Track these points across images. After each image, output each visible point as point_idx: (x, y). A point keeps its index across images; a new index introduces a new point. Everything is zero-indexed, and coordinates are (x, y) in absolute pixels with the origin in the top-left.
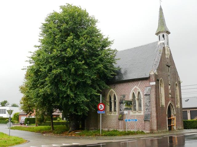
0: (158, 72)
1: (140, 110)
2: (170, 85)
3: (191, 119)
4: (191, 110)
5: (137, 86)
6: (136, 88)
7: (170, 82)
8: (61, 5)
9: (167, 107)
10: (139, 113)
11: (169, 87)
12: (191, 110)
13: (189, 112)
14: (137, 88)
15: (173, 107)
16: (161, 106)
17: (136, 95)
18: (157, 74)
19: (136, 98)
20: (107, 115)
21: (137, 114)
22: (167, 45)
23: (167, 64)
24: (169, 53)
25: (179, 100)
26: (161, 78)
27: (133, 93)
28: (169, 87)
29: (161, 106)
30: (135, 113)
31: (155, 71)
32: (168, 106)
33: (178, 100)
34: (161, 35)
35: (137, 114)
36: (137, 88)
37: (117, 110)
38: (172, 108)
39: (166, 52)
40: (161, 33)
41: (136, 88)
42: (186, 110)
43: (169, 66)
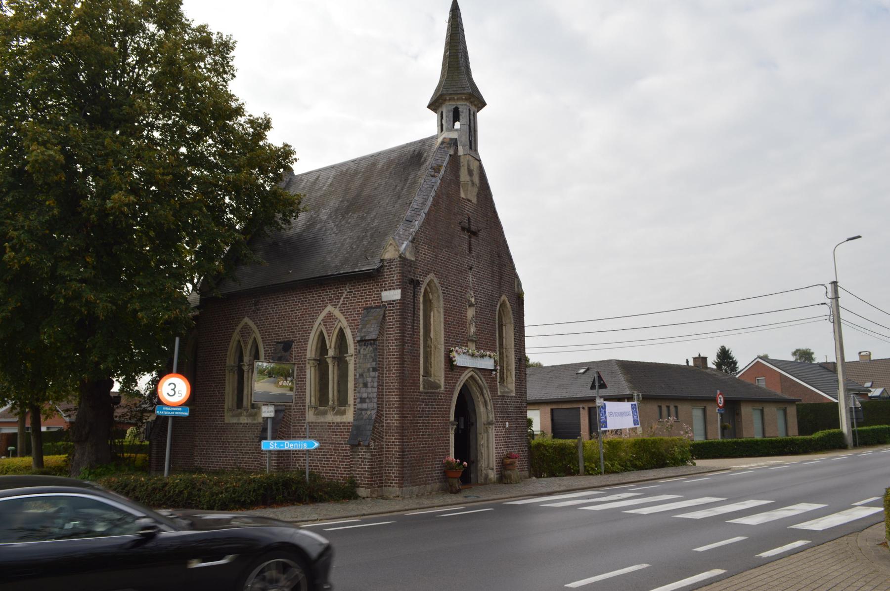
0: (416, 250)
1: (343, 400)
2: (471, 305)
3: (801, 431)
4: (554, 407)
5: (335, 306)
6: (330, 315)
7: (472, 292)
8: (794, 350)
9: (453, 389)
10: (336, 414)
11: (471, 313)
12: (554, 407)
13: (586, 408)
14: (337, 313)
15: (482, 394)
16: (421, 389)
17: (331, 343)
18: (409, 256)
19: (331, 353)
20: (226, 421)
21: (330, 418)
22: (468, 147)
23: (467, 225)
24: (476, 179)
25: (513, 367)
26: (431, 276)
27: (322, 332)
28: (471, 313)
29: (421, 389)
30: (324, 413)
31: (404, 246)
32: (458, 389)
33: (508, 365)
34: (447, 109)
35: (330, 418)
36: (337, 313)
37: (351, 400)
38: (481, 399)
39: (464, 176)
40: (447, 103)
41: (330, 315)
42: (575, 406)
43: (475, 234)
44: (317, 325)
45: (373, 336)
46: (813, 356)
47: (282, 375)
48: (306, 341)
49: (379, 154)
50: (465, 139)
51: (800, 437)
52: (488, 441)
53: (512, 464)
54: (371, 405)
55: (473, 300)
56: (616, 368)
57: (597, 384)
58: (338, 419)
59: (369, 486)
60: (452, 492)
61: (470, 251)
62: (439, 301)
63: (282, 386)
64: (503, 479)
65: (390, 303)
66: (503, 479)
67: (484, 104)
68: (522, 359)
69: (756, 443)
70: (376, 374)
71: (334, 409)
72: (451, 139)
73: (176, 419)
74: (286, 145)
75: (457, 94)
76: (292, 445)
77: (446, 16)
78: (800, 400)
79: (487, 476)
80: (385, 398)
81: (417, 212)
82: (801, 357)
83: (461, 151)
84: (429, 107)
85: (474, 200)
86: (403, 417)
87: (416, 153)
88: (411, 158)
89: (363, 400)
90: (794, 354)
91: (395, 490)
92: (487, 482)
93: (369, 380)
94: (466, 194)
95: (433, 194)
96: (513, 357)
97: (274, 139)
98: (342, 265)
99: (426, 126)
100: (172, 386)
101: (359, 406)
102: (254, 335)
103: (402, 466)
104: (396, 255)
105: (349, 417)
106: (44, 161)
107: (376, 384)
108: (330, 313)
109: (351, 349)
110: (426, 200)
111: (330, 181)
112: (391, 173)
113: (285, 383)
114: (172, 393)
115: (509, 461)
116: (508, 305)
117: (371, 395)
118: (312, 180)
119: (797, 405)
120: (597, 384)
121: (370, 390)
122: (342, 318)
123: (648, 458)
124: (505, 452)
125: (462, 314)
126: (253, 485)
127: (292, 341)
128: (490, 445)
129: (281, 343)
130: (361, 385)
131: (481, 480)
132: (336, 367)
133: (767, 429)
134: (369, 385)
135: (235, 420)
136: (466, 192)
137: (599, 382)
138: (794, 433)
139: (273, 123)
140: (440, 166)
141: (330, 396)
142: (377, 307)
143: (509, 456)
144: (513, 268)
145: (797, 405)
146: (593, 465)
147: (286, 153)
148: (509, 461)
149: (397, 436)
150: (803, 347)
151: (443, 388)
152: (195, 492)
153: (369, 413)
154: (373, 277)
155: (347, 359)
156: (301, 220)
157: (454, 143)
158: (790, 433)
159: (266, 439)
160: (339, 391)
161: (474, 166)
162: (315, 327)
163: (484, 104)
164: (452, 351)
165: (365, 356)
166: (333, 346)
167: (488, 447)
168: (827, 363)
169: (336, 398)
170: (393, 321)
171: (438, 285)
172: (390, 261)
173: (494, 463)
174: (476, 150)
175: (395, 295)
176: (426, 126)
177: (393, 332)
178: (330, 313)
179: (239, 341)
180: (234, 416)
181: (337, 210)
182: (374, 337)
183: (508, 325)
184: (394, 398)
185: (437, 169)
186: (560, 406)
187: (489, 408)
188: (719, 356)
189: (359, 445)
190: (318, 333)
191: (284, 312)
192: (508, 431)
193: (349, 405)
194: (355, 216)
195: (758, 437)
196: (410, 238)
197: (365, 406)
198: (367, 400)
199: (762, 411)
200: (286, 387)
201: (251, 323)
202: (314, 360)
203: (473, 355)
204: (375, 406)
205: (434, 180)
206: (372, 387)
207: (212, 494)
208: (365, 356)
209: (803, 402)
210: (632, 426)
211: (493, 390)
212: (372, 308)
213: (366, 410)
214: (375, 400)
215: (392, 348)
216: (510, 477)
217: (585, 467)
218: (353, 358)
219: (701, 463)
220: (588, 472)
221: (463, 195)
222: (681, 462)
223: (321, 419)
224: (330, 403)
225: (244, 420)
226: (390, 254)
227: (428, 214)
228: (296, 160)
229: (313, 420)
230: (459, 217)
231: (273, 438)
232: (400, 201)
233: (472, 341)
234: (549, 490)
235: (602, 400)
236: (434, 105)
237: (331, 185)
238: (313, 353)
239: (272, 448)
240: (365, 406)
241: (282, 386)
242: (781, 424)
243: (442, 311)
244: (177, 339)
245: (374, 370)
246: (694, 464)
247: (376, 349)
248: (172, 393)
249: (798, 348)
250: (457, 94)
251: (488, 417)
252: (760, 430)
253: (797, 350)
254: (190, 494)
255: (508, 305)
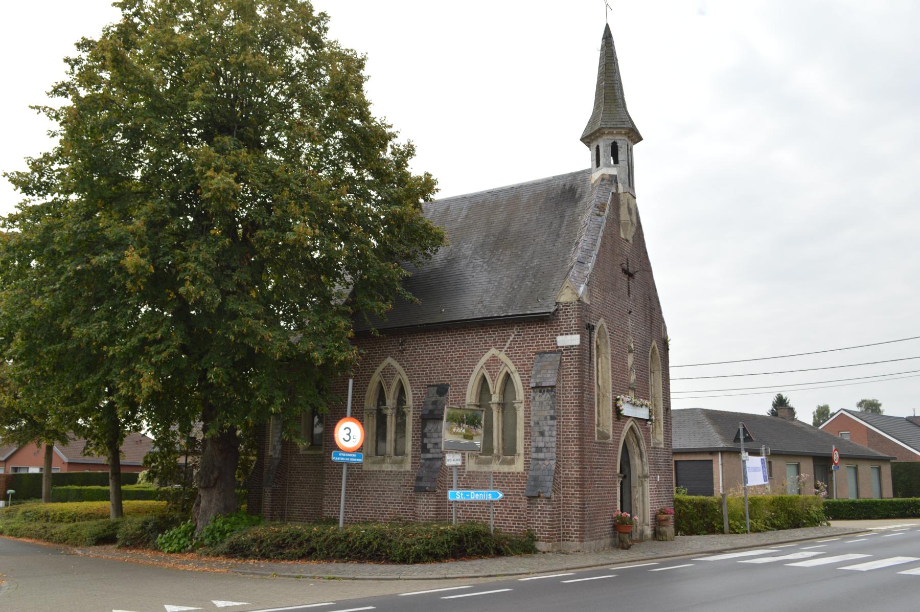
1: (510, 450)
2: (631, 351)
5: (500, 349)
6: (494, 359)
7: (631, 338)
11: (630, 359)
14: (502, 356)
15: (639, 445)
18: (586, 300)
19: (495, 398)
26: (602, 321)
28: (630, 359)
30: (488, 462)
34: (604, 144)
36: (502, 356)
38: (637, 450)
40: (605, 137)
41: (494, 359)
44: (478, 369)
45: (551, 383)
46: (881, 408)
47: (455, 421)
48: (465, 386)
49: (521, 187)
50: (623, 176)
51: (895, 499)
52: (643, 495)
53: (666, 520)
54: (548, 455)
55: (632, 346)
56: (703, 417)
57: (742, 437)
58: (505, 469)
59: (549, 540)
60: (623, 548)
61: (629, 294)
62: (607, 347)
63: (455, 433)
64: (657, 535)
65: (567, 348)
66: (657, 535)
67: (640, 139)
68: (667, 409)
69: (875, 504)
70: (555, 423)
71: (499, 457)
72: (611, 176)
73: (350, 465)
74: (428, 175)
75: (611, 128)
76: (477, 495)
77: (598, 42)
78: (895, 458)
79: (642, 533)
80: (563, 448)
81: (587, 252)
82: (867, 409)
83: (621, 190)
84: (583, 140)
85: (631, 241)
86: (583, 468)
87: (567, 187)
88: (564, 194)
89: (539, 450)
90: (860, 405)
91: (576, 544)
92: (642, 539)
93: (547, 428)
94: (625, 234)
95: (601, 234)
96: (662, 406)
97: (415, 168)
98: (508, 306)
99: (580, 159)
100: (348, 431)
101: (534, 455)
102: (398, 377)
103: (583, 520)
104: (574, 299)
105: (519, 466)
106: (224, 190)
107: (554, 433)
108: (494, 356)
109: (520, 394)
110: (595, 240)
111: (464, 213)
112: (541, 208)
113: (459, 430)
114: (347, 438)
115: (664, 517)
116: (657, 352)
117: (549, 445)
118: (441, 210)
119: (892, 464)
120: (742, 437)
121: (547, 439)
122: (509, 362)
123: (786, 517)
124: (657, 508)
125: (624, 359)
126: (445, 537)
127: (448, 385)
128: (646, 499)
129: (434, 386)
130: (537, 434)
131: (636, 536)
132: (500, 414)
133: (861, 489)
134: (546, 434)
135: (376, 468)
136: (625, 231)
137: (744, 435)
138: (888, 494)
139: (417, 151)
140: (604, 205)
141: (495, 443)
142: (551, 352)
143: (662, 512)
144: (661, 313)
145: (892, 464)
146: (738, 523)
147: (428, 185)
148: (664, 517)
149: (577, 488)
150: (869, 397)
151: (611, 439)
152: (385, 543)
153: (547, 462)
154: (545, 320)
155: (516, 405)
156: (440, 255)
157: (613, 179)
158: (885, 495)
159: (451, 487)
160: (503, 439)
161: (632, 206)
162: (477, 369)
163: (639, 139)
164: (618, 400)
165: (541, 403)
166: (497, 391)
167: (643, 501)
168: (914, 417)
169: (501, 447)
170: (571, 367)
171: (607, 330)
172: (567, 305)
173: (649, 519)
174: (633, 188)
175: (574, 340)
176: (580, 159)
177: (572, 380)
178: (494, 356)
179: (380, 383)
180: (374, 463)
181: (482, 246)
182: (552, 384)
183: (657, 372)
184: (573, 448)
185: (601, 207)
186: (684, 458)
187: (644, 460)
188: (775, 406)
189: (539, 496)
190: (479, 377)
191: (436, 356)
192: (659, 485)
193: (519, 455)
194: (508, 252)
195: (852, 498)
196: (586, 281)
197: (541, 455)
198: (544, 450)
199: (856, 469)
200: (460, 434)
201: (395, 364)
202: (499, 404)
203: (634, 404)
204: (554, 455)
205: (600, 219)
206: (551, 436)
207: (406, 545)
208: (541, 403)
209: (899, 460)
210: (763, 482)
211: (648, 441)
212: (545, 353)
213: (543, 460)
214: (554, 450)
215: (571, 395)
216: (664, 533)
217: (730, 525)
218: (522, 405)
219: (835, 524)
220: (733, 531)
221: (622, 236)
222: (814, 522)
223: (485, 469)
224: (495, 451)
225: (387, 467)
226: (566, 297)
227: (598, 256)
228: (437, 190)
229: (475, 470)
230: (621, 258)
231: (459, 488)
232: (560, 240)
233: (633, 389)
234: (712, 548)
235: (747, 454)
236: (587, 139)
237: (467, 217)
238: (474, 398)
239: (458, 499)
240: (541, 455)
241: (455, 433)
242: (875, 485)
243: (610, 357)
244: (351, 381)
245: (553, 418)
246: (829, 524)
247: (555, 396)
248: (347, 438)
249: (864, 398)
250: (611, 128)
251: (643, 469)
252: (854, 490)
253: (863, 401)
254: (380, 545)
255: (657, 352)
